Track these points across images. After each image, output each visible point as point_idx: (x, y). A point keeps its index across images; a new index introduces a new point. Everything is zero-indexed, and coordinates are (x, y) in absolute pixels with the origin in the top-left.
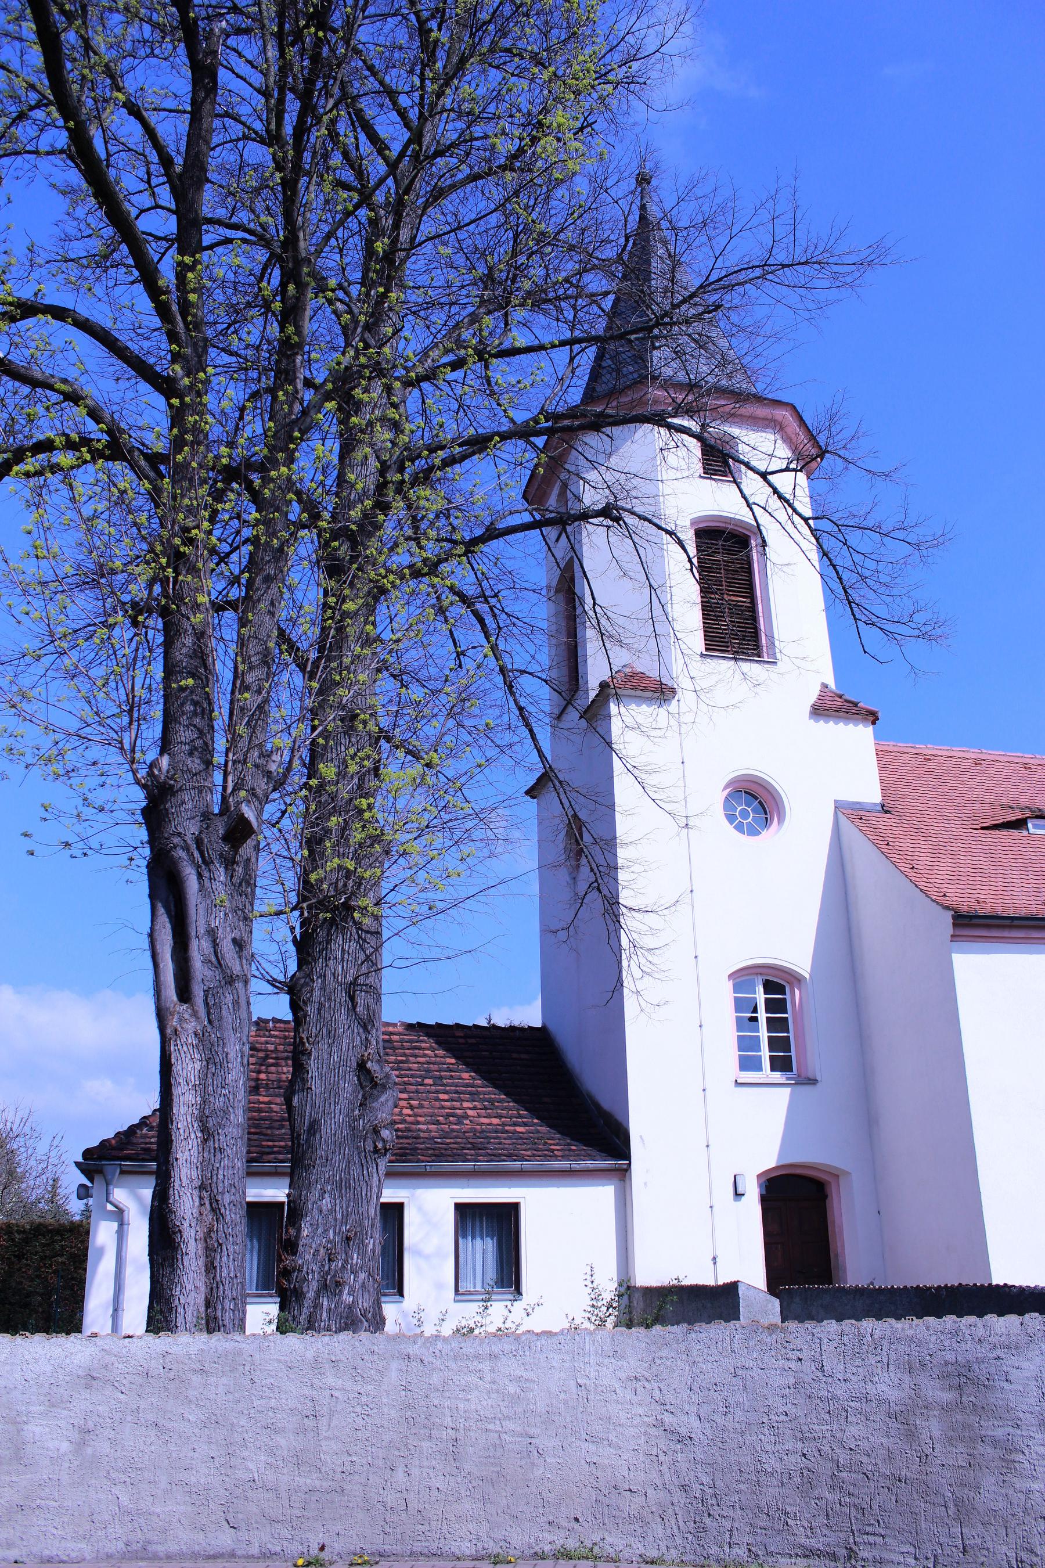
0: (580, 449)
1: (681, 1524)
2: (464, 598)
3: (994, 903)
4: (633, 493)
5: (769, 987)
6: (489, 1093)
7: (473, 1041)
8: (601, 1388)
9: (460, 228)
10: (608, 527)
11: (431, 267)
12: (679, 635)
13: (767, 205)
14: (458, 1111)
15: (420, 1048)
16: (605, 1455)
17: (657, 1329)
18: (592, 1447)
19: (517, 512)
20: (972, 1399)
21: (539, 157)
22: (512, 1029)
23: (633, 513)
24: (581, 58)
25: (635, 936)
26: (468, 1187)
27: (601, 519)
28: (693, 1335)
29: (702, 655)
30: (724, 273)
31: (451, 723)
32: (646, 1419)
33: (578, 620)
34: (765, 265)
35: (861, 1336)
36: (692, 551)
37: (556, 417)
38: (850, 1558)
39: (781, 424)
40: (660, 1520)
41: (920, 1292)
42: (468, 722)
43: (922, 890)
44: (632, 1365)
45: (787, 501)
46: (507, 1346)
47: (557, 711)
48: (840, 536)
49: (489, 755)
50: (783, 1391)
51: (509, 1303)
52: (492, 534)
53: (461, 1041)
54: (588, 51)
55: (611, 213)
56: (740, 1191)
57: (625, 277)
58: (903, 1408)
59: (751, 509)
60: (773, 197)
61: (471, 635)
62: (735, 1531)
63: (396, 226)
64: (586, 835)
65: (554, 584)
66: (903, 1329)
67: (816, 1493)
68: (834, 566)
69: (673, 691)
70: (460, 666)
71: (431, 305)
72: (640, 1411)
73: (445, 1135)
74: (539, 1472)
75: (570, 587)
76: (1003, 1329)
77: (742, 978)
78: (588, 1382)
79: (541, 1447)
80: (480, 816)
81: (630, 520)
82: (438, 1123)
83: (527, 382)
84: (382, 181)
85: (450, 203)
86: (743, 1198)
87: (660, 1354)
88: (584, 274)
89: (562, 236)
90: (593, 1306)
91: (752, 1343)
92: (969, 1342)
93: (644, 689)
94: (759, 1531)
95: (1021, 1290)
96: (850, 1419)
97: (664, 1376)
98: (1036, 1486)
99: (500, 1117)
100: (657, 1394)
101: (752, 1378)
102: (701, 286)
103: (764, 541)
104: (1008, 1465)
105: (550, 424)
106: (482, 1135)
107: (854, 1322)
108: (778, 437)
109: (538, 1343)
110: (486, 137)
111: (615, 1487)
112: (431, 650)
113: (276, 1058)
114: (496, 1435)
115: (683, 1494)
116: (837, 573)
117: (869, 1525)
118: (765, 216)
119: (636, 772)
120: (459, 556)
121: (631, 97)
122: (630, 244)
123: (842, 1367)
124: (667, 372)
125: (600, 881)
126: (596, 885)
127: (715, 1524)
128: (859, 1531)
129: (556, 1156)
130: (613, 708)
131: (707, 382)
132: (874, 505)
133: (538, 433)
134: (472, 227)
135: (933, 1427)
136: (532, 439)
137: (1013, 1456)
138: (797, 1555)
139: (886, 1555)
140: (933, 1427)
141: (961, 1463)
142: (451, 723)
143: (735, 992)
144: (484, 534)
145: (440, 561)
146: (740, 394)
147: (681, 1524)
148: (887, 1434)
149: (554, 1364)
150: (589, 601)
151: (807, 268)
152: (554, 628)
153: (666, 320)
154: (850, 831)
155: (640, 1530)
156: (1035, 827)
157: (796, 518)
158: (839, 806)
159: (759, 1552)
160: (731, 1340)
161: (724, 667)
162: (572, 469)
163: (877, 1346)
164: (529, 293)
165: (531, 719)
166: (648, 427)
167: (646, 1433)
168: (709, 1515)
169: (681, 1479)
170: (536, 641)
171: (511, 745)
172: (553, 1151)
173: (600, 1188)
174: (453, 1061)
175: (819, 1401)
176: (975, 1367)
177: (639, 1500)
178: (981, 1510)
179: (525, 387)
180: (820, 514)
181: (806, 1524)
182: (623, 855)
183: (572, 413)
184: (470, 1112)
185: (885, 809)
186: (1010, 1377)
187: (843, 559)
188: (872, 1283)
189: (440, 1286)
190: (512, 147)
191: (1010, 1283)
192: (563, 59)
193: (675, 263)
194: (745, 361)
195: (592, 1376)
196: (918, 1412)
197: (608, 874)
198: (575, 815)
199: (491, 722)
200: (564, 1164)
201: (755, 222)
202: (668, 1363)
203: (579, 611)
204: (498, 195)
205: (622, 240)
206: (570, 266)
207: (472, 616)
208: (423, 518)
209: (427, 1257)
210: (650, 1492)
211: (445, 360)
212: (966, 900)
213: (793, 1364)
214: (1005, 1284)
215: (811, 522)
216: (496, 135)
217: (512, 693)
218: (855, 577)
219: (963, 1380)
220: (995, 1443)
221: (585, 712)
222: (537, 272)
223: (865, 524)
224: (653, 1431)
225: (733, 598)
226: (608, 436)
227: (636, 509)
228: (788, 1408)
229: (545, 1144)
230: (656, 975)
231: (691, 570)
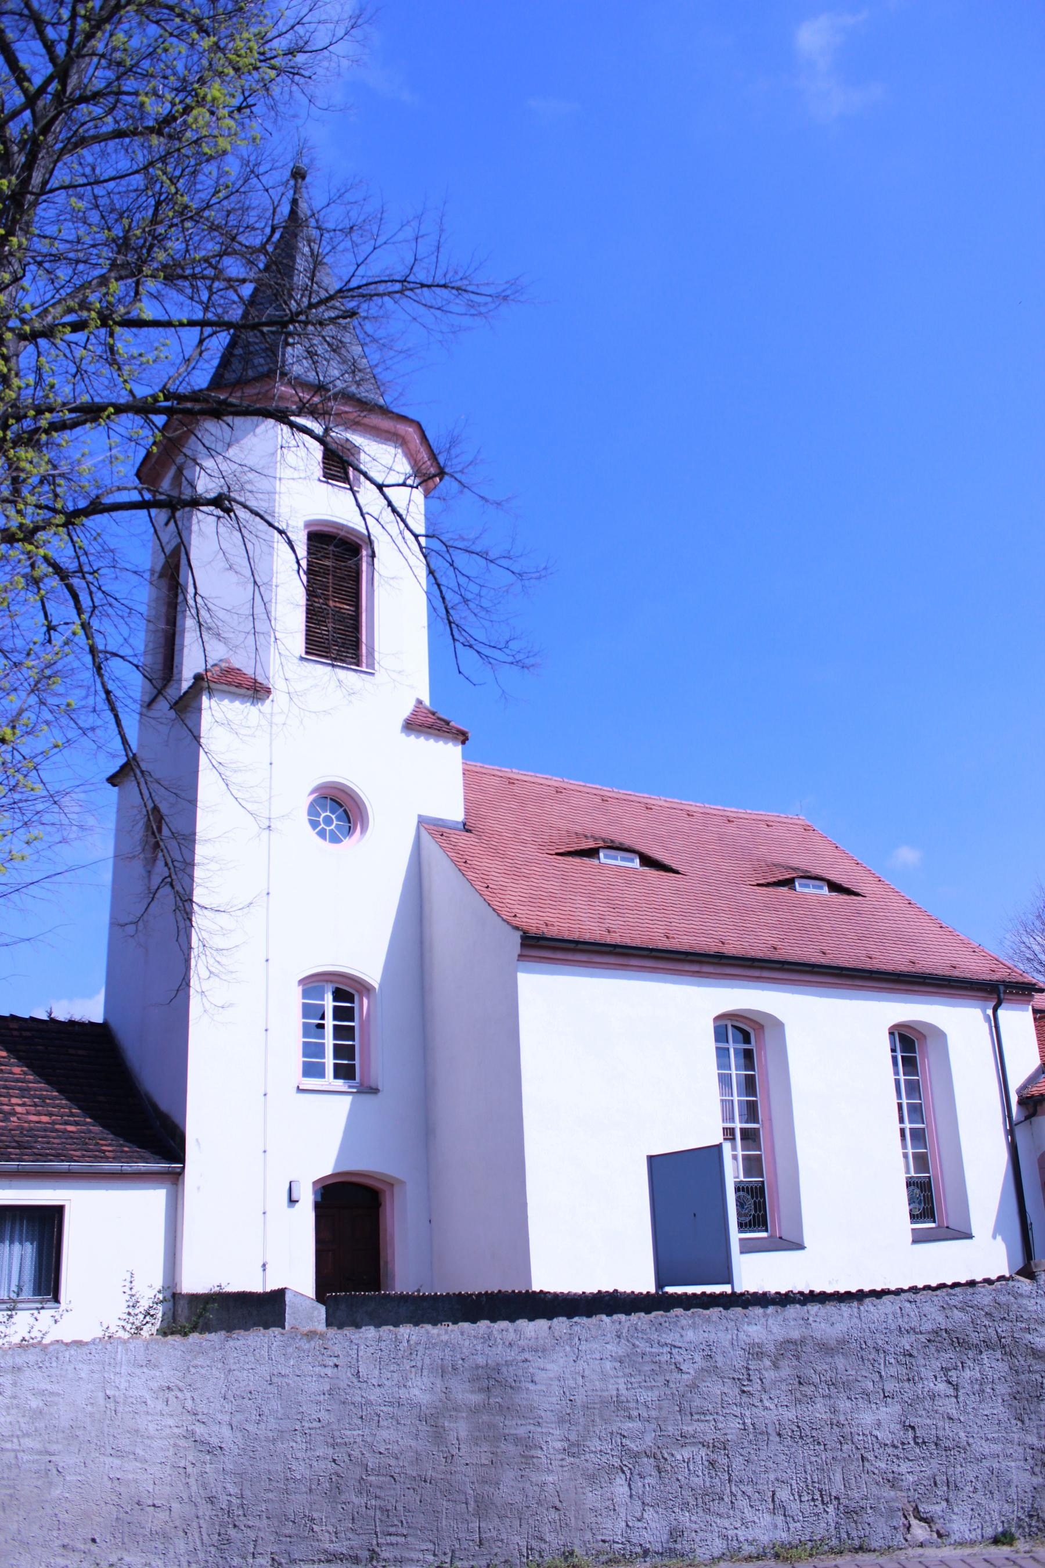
0: (200, 436)
1: (205, 1537)
2: (57, 569)
3: (560, 926)
4: (248, 487)
5: (339, 995)
6: (41, 1090)
7: (28, 1034)
8: (131, 1400)
9: (97, 182)
10: (219, 517)
11: (62, 218)
12: (278, 635)
13: (412, 223)
14: (5, 1107)
16: (130, 1469)
17: (194, 1337)
18: (117, 1462)
19: (125, 489)
20: (499, 1400)
21: (190, 127)
22: (72, 1023)
23: (245, 507)
24: (245, 35)
25: (205, 935)
26: (10, 1188)
27: (212, 508)
28: (231, 1343)
29: (302, 658)
30: (364, 282)
31: (33, 700)
32: (176, 1430)
33: (179, 608)
34: (405, 281)
35: (397, 1341)
36: (302, 551)
37: (181, 398)
38: (372, 1559)
39: (403, 438)
40: (183, 1534)
41: (462, 1299)
42: (51, 701)
43: (494, 910)
44: (166, 1374)
45: (400, 516)
46: (31, 1357)
47: (147, 699)
48: (447, 557)
49: (69, 736)
50: (318, 1398)
51: (36, 1312)
52: (96, 508)
53: (16, 1033)
54: (254, 30)
55: (259, 200)
56: (294, 1197)
57: (267, 268)
58: (433, 1411)
59: (364, 519)
60: (419, 218)
61: (62, 610)
62: (260, 1541)
63: (29, 166)
64: (165, 829)
65: (158, 568)
66: (439, 1335)
67: (343, 1498)
68: (439, 585)
69: (268, 691)
70: (50, 641)
71: (56, 258)
72: (171, 1422)
74: (56, 1492)
75: (172, 574)
76: (533, 1334)
77: (312, 984)
78: (117, 1393)
79: (61, 1464)
80: (53, 798)
81: (242, 513)
83: (150, 357)
84: (15, 114)
85: (87, 154)
86: (297, 1205)
87: (195, 1362)
88: (225, 258)
89: (206, 214)
90: (129, 1314)
91: (290, 1350)
92: (500, 1346)
93: (239, 686)
94: (284, 1539)
95: (556, 1296)
96: (381, 1423)
97: (198, 1385)
98: (551, 1479)
99: (50, 1114)
100: (189, 1404)
101: (288, 1385)
102: (340, 291)
103: (373, 552)
104: (528, 1460)
105: (168, 404)
106: (30, 1133)
107: (391, 1328)
108: (400, 451)
109: (67, 1354)
110: (136, 94)
111: (138, 1504)
112: (18, 620)
114: (13, 1454)
115: (210, 1506)
116: (441, 592)
117: (392, 1526)
118: (409, 233)
119: (221, 769)
120: (57, 526)
121: (295, 88)
122: (277, 236)
123: (377, 1372)
124: (297, 370)
125: (174, 877)
126: (169, 880)
127: (240, 1535)
128: (383, 1533)
129: (107, 1157)
130: (205, 700)
131: (335, 386)
132: (484, 531)
133: (158, 411)
134: (111, 185)
135: (459, 1428)
136: (151, 416)
137: (533, 1452)
138: (320, 1561)
139: (407, 1554)
140: (459, 1428)
141: (484, 1461)
142: (33, 700)
143: (304, 997)
144: (88, 507)
145: (37, 529)
146: (366, 403)
147: (205, 1537)
148: (416, 1437)
149: (83, 1375)
150: (191, 590)
151: (444, 290)
152: (153, 612)
153: (302, 318)
154: (430, 845)
155: (161, 1547)
156: (606, 857)
157: (407, 534)
158: (423, 822)
159: (283, 1561)
160: (269, 1347)
161: (321, 672)
162: (189, 453)
163: (412, 1351)
164: (165, 267)
165: (118, 704)
166: (271, 422)
167: (175, 1445)
168: (235, 1526)
169: (208, 1491)
170: (132, 625)
171: (93, 729)
172: (104, 1152)
173: (151, 1191)
175: (352, 1407)
176: (504, 1369)
177: (163, 1515)
178: (499, 1504)
179: (148, 362)
180: (430, 533)
181: (331, 1529)
182: (201, 851)
183: (195, 396)
184: (19, 1109)
185: (466, 828)
186: (535, 1379)
187: (448, 579)
188: (419, 1291)
190: (163, 109)
191: (546, 1290)
192: (229, 32)
193: (317, 262)
194: (376, 371)
195: (122, 1387)
196: (447, 1415)
197: (183, 870)
198: (156, 809)
199: (73, 703)
200: (115, 1166)
201: (401, 236)
202: (203, 1371)
203: (181, 598)
204: (141, 158)
205: (268, 230)
206: (211, 247)
207: (66, 591)
208: (24, 481)
210: (175, 1506)
211: (68, 318)
212: (535, 921)
213: (329, 1371)
214: (541, 1291)
215: (422, 540)
216: (146, 94)
217: (101, 676)
218: (457, 599)
219: (492, 1382)
220: (517, 1440)
221: (176, 703)
222: (176, 246)
223: (473, 548)
224: (182, 1443)
225: (338, 605)
226: (228, 425)
227: (248, 503)
228: (323, 1415)
229: (97, 1144)
230: (224, 977)
231: (298, 572)
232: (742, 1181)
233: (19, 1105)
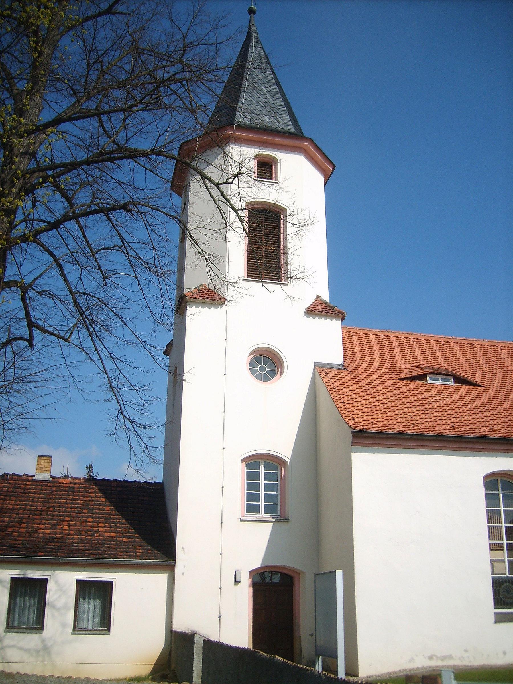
6: (117, 519)
7: (120, 489)
15: (88, 492)
73: (82, 541)
82: (81, 534)
113: (5, 496)
125: (123, 409)
161: (256, 287)
174: (104, 500)
184: (101, 529)
185: (344, 368)
189: (64, 625)
209: (58, 609)
232: (507, 577)
233: (102, 527)
